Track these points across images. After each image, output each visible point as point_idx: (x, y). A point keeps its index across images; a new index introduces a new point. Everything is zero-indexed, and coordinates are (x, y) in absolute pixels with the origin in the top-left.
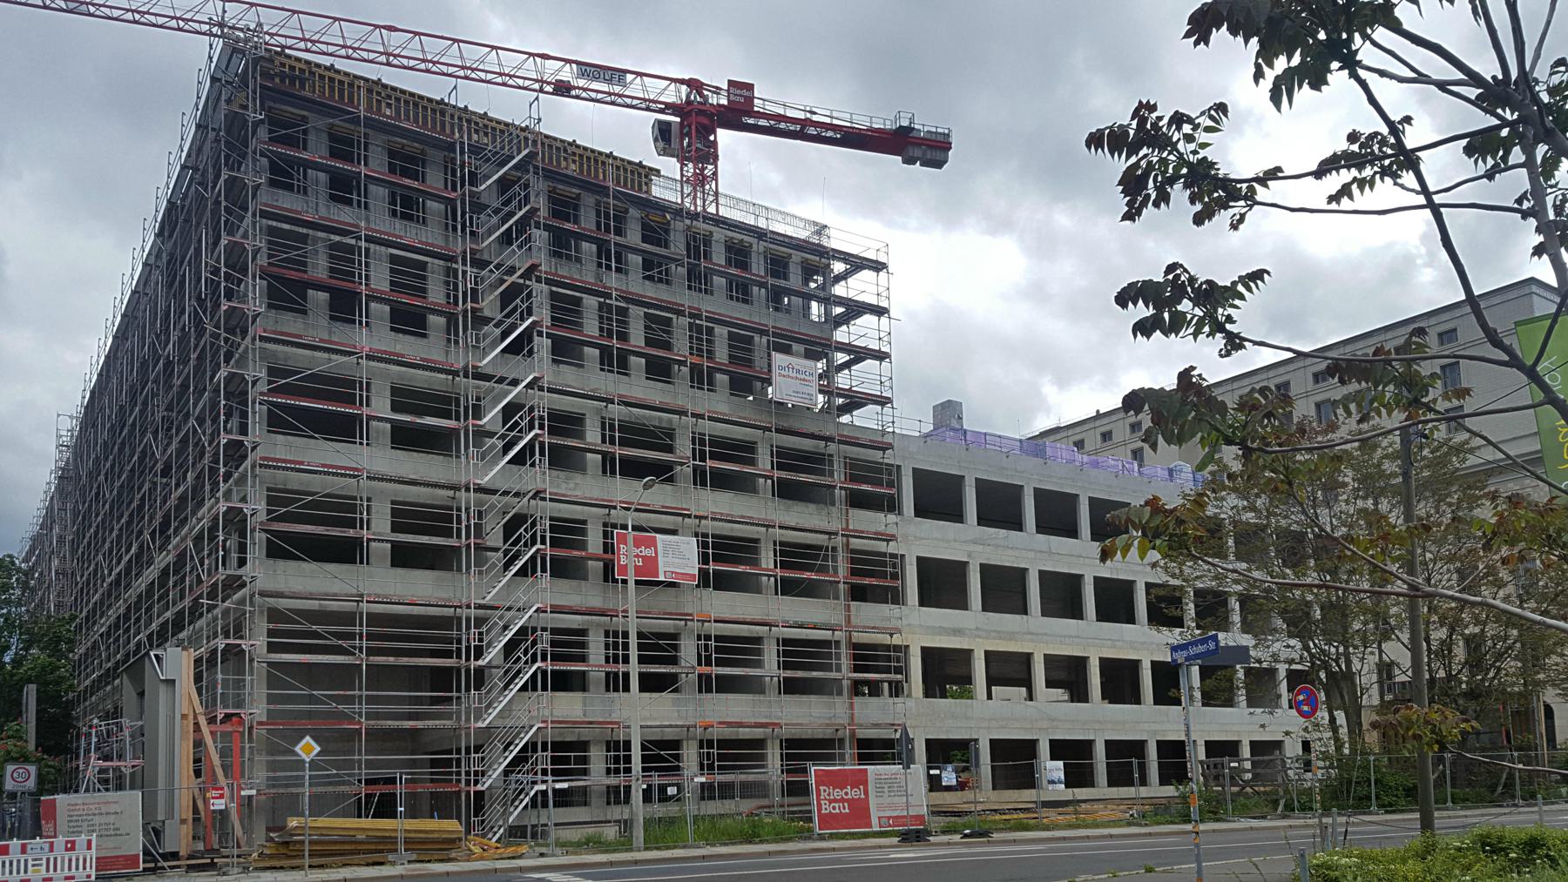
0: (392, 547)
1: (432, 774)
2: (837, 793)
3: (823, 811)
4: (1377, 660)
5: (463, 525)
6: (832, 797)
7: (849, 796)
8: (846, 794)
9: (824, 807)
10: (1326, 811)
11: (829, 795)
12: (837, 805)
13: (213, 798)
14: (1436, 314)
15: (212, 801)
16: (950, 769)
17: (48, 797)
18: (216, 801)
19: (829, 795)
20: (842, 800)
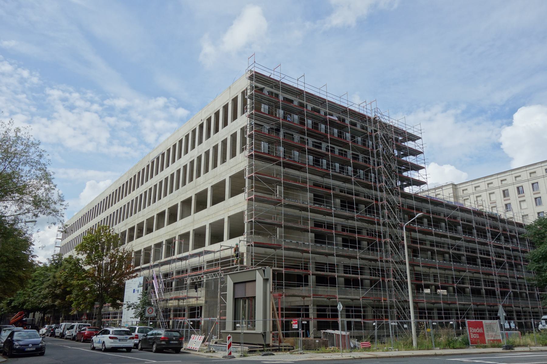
0: (345, 279)
1: (297, 284)
2: (475, 330)
3: (471, 337)
4: (62, 331)
5: (353, 187)
6: (473, 332)
7: (479, 332)
8: (477, 330)
9: (471, 335)
10: (428, 319)
11: (472, 331)
12: (475, 335)
13: (294, 324)
14: (544, 163)
15: (293, 325)
16: (512, 322)
17: (207, 319)
18: (295, 325)
19: (472, 331)
20: (477, 333)
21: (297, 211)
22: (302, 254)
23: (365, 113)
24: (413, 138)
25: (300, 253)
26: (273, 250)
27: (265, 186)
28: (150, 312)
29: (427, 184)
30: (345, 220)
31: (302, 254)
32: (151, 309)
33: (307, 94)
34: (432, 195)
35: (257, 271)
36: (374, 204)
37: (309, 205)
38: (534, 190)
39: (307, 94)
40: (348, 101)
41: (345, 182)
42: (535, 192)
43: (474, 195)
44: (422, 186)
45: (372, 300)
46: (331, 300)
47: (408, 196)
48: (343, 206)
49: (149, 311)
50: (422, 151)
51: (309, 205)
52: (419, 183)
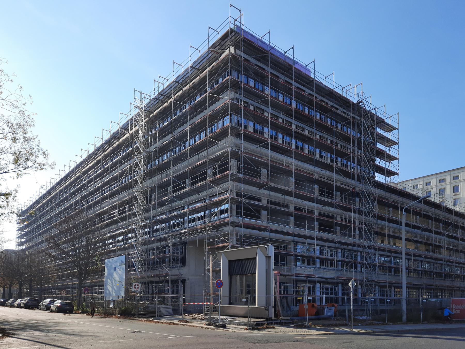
21: (279, 195)
22: (285, 236)
23: (349, 97)
24: (390, 128)
25: (282, 235)
26: (257, 232)
27: (255, 168)
28: (136, 288)
29: (398, 175)
30: (322, 206)
31: (285, 236)
32: (137, 285)
33: (125, 133)
34: (399, 187)
35: (222, 253)
36: (351, 192)
37: (292, 188)
38: (454, 192)
39: (125, 133)
40: (334, 82)
41: (324, 169)
42: (454, 194)
43: (451, 184)
44: (392, 177)
45: (342, 279)
46: (309, 278)
47: (381, 186)
48: (321, 192)
49: (135, 286)
50: (398, 142)
51: (292, 188)
52: (389, 173)
